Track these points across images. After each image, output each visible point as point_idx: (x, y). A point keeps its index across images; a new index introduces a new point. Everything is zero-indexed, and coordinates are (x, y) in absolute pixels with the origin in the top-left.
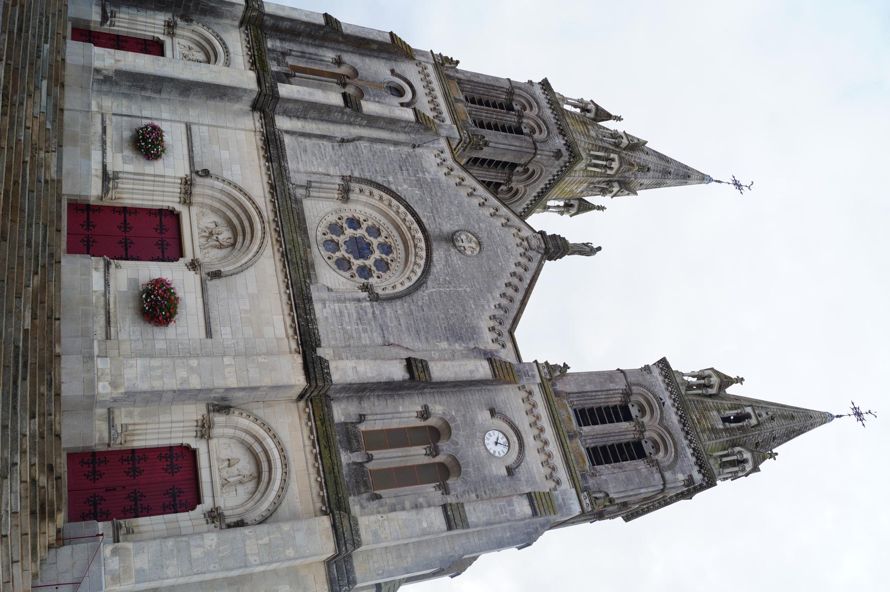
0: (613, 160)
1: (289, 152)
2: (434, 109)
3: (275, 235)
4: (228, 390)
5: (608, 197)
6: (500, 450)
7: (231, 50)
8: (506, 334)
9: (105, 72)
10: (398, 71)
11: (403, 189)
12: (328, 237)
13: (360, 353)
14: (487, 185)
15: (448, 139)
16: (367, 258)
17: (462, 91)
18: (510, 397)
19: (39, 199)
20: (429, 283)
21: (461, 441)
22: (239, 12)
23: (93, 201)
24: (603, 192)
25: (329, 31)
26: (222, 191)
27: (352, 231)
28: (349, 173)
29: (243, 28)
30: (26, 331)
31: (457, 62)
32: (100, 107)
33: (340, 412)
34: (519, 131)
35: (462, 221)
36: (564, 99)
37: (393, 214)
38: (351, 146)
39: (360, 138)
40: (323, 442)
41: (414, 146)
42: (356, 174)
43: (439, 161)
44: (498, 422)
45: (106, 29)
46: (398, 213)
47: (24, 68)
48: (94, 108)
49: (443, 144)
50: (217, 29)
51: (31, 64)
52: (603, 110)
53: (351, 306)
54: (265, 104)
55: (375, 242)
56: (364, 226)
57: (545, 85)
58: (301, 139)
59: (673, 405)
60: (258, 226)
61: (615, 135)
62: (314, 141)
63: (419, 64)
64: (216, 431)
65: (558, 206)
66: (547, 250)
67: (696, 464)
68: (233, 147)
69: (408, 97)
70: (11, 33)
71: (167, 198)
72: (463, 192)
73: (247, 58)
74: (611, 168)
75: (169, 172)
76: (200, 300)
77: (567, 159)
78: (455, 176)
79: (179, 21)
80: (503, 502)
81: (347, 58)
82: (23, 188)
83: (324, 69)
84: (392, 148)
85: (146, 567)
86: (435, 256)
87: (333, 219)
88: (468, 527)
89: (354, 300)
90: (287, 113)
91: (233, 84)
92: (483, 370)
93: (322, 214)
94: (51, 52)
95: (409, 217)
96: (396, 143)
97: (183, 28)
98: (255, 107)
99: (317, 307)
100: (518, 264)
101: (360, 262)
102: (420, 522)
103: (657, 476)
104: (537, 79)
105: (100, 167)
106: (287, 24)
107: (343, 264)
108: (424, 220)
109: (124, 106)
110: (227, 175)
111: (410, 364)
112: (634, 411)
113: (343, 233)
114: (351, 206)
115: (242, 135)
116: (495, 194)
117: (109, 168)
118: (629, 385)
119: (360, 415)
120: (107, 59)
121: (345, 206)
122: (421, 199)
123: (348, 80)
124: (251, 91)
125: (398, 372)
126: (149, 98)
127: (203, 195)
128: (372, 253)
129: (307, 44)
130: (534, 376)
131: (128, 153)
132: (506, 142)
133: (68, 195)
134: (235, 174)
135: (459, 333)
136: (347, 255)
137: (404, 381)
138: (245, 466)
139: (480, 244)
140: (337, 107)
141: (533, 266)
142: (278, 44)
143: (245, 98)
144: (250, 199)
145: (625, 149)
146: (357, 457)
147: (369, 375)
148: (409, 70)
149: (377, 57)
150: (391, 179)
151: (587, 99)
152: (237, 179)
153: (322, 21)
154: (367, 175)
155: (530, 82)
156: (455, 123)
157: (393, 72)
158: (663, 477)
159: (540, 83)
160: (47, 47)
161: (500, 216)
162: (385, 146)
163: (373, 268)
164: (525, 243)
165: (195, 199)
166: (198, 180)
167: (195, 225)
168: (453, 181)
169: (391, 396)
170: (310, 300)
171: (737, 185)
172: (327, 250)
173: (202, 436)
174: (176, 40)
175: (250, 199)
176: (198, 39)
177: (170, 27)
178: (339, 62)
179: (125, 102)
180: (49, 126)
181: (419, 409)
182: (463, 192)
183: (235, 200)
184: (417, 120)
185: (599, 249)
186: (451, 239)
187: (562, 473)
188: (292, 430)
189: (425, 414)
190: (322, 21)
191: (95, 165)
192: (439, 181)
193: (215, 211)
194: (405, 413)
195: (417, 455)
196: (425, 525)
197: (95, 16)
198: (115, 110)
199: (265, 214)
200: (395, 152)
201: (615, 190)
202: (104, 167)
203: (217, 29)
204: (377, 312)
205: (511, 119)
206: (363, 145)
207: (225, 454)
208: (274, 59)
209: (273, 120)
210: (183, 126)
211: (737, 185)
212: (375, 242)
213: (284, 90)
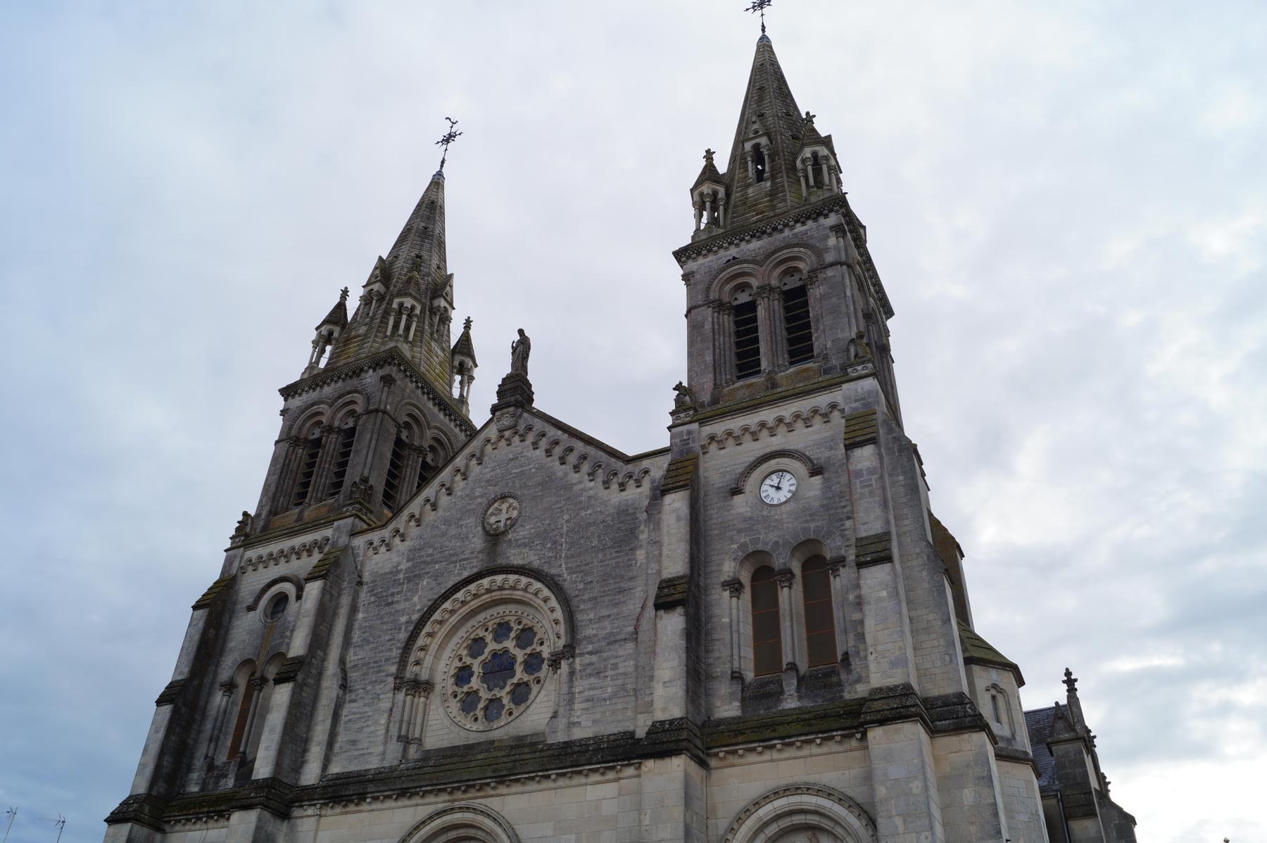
0: (401, 305)
1: (354, 767)
3: (473, 793)
5: (454, 314)
8: (630, 467)
10: (250, 601)
11: (419, 601)
12: (480, 713)
13: (645, 674)
14: (424, 481)
15: (354, 534)
16: (514, 658)
17: (287, 509)
18: (718, 466)
21: (773, 537)
24: (445, 319)
25: (182, 700)
28: (391, 680)
29: (167, 827)
31: (245, 514)
33: (727, 708)
34: (351, 433)
35: (470, 521)
36: (312, 366)
37: (454, 619)
38: (353, 675)
39: (342, 661)
40: (767, 734)
41: (360, 583)
42: (393, 669)
43: (383, 549)
44: (750, 485)
46: (452, 612)
49: (359, 542)
52: (331, 314)
53: (579, 685)
55: (485, 695)
56: (468, 660)
59: (737, 245)
60: (458, 817)
61: (366, 300)
62: (341, 729)
63: (243, 570)
65: (461, 383)
66: (518, 405)
67: (815, 220)
69: (289, 588)
72: (430, 517)
74: (413, 308)
77: (395, 369)
78: (407, 527)
80: (857, 483)
81: (224, 674)
83: (237, 709)
84: (360, 616)
86: (517, 561)
87: (454, 706)
88: (888, 534)
92: (676, 503)
93: (447, 722)
95: (460, 595)
96: (354, 609)
98: (284, 814)
100: (535, 446)
101: (519, 669)
102: (880, 600)
104: (280, 403)
106: (167, 760)
107: (521, 695)
108: (466, 574)
111: (663, 605)
112: (743, 298)
114: (438, 679)
116: (437, 470)
118: (708, 303)
119: (733, 678)
121: (438, 688)
122: (436, 577)
123: (257, 675)
124: (259, 819)
125: (673, 624)
129: (199, 732)
130: (689, 433)
132: (364, 452)
135: (625, 531)
136: (508, 688)
137: (686, 614)
139: (503, 498)
141: (538, 424)
142: (195, 776)
145: (387, 288)
146: (790, 685)
147: (675, 663)
148: (251, 583)
150: (403, 619)
151: (313, 335)
153: (167, 709)
154: (396, 653)
155: (283, 413)
157: (251, 608)
158: (832, 265)
159: (286, 400)
161: (467, 466)
162: (356, 625)
163: (528, 650)
164: (507, 434)
168: (413, 531)
169: (708, 633)
170: (567, 744)
171: (449, 138)
172: (498, 717)
178: (230, 687)
182: (430, 517)
184: (323, 577)
185: (521, 332)
186: (494, 537)
192: (413, 550)
194: (732, 614)
195: (790, 599)
196: (884, 594)
199: (440, 806)
200: (366, 611)
201: (443, 303)
204: (590, 648)
205: (333, 443)
206: (352, 657)
208: (217, 782)
211: (449, 138)
212: (492, 646)
213: (263, 769)
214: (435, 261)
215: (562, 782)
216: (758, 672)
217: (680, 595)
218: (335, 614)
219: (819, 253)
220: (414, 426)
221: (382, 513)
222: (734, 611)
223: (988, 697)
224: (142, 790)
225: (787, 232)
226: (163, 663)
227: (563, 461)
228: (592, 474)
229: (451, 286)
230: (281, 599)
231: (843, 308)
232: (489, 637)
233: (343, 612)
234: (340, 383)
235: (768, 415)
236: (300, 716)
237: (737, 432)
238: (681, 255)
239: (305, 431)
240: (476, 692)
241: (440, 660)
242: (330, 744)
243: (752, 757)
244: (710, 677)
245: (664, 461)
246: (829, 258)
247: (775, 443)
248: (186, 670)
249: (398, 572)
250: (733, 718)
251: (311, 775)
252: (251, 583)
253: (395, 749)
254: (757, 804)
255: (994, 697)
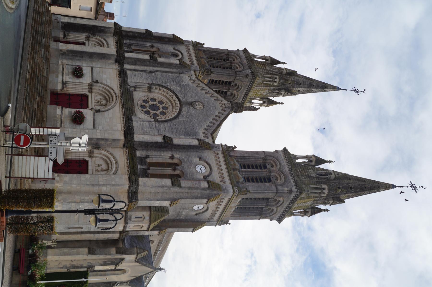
1: (128, 76)
2: (190, 61)
3: (120, 101)
4: (98, 139)
6: (203, 170)
7: (109, 44)
9: (63, 51)
10: (177, 48)
11: (173, 87)
12: (143, 104)
13: (144, 133)
14: (218, 92)
15: (195, 71)
17: (206, 55)
18: (209, 155)
19: (40, 79)
20: (180, 117)
21: (186, 166)
22: (113, 30)
23: (59, 91)
24: (278, 94)
25: (148, 35)
26: (103, 87)
27: (152, 102)
28: (151, 82)
29: (115, 37)
30: (35, 109)
31: (204, 44)
32: (62, 62)
33: (139, 154)
34: (231, 68)
35: (197, 98)
36: (255, 57)
37: (168, 96)
38: (153, 74)
39: (157, 71)
40: (130, 159)
41: (180, 74)
42: (154, 83)
43: (190, 78)
44: (202, 162)
45: (65, 39)
46: (170, 95)
47: (37, 44)
48: (60, 63)
49: (192, 72)
50: (104, 37)
51: (39, 43)
53: (147, 123)
54: (120, 60)
55: (161, 106)
56: (157, 101)
57: (245, 51)
58: (133, 72)
59: (287, 164)
60: (115, 98)
61: (280, 69)
62: (139, 72)
63: (186, 45)
64: (95, 155)
66: (232, 108)
67: (295, 185)
68: (109, 75)
69: (180, 57)
70: (33, 34)
71: (84, 91)
73: (115, 46)
74: (276, 82)
75: (84, 82)
76: (92, 119)
77: (251, 78)
78: (196, 83)
79: (91, 35)
81: (155, 45)
82: (36, 74)
83: (147, 49)
84: (170, 74)
85: (67, 180)
86: (183, 109)
87: (145, 98)
89: (148, 121)
90: (129, 63)
91: (107, 53)
92: (195, 142)
93: (140, 97)
94: (45, 42)
95: (174, 96)
96: (172, 73)
97: (92, 38)
98: (116, 61)
99: (134, 123)
100: (219, 113)
102: (162, 182)
103: (274, 187)
104: (241, 48)
105: (61, 80)
106: (131, 34)
107: (147, 113)
109: (70, 62)
110: (104, 82)
111: (164, 137)
112: (268, 166)
113: (148, 103)
114: (153, 94)
115: (111, 71)
116: (225, 98)
117: (64, 80)
119: (147, 155)
120: (64, 47)
121: (150, 94)
122: (180, 91)
123: (155, 53)
124: (114, 55)
125: (159, 139)
126: (79, 60)
127: (96, 89)
128: (159, 109)
129: (140, 41)
130: (219, 148)
131: (70, 76)
132: (222, 72)
133: (51, 89)
134: (108, 82)
136: (149, 110)
137: (161, 143)
138: (104, 166)
139: (203, 106)
140: (147, 60)
141: (226, 113)
142: (128, 41)
143: (112, 58)
144: (112, 89)
145: (285, 75)
146: (144, 167)
147: (149, 139)
148: (182, 49)
149: (168, 44)
150: (168, 84)
151: (267, 55)
152: (108, 84)
153: (144, 32)
156: (199, 65)
157: (174, 49)
158: (277, 188)
160: (44, 40)
161: (214, 97)
162: (167, 74)
163: (159, 114)
164: (224, 106)
165: (94, 91)
166: (95, 84)
167: (92, 100)
168: (195, 85)
169: (159, 151)
171: (356, 91)
172: (142, 108)
173: (90, 157)
174: (90, 42)
175: (112, 89)
176: (98, 41)
177: (88, 38)
178: (152, 47)
179: (70, 61)
180: (44, 61)
181: (170, 155)
182: (199, 89)
183: (107, 90)
184: (180, 64)
186: (191, 104)
187: (227, 180)
188: (121, 156)
189: (172, 158)
190: (144, 32)
191: (60, 79)
192: (189, 85)
193: (101, 95)
194: (165, 156)
195: (169, 171)
196: (163, 183)
197: (62, 36)
198: (67, 63)
200: (171, 76)
201: (331, 202)
202: (63, 80)
203: (104, 37)
204: (157, 125)
206: (158, 73)
207: (98, 162)
208: (126, 46)
209: (123, 66)
210: (90, 68)
211: (356, 91)
212: (161, 106)
213: (127, 55)
214: (301, 89)
215: (122, 119)
216: (149, 163)
217: (167, 144)
218: (171, 68)
219: (282, 185)
220: (236, 87)
221: (205, 79)
222: (165, 157)
223: (141, 216)
224: (123, 29)
225: (291, 178)
226: (158, 29)
227: (214, 119)
228: (208, 126)
229: (291, 95)
230: (177, 56)
231: (260, 189)
232: (163, 105)
233: (171, 70)
234: (247, 64)
235: (224, 167)
236: (142, 62)
237: (218, 160)
238: (285, 150)
239: (232, 56)
240: (148, 103)
241: (158, 94)
242: (135, 70)
243: (125, 157)
244: (147, 150)
245: (211, 142)
246: (279, 188)
247: (215, 169)
248: (155, 35)
249: (182, 82)
250: (136, 154)
251: (127, 66)
252: (182, 49)
253: (133, 84)
254: (114, 157)
255: (141, 217)
